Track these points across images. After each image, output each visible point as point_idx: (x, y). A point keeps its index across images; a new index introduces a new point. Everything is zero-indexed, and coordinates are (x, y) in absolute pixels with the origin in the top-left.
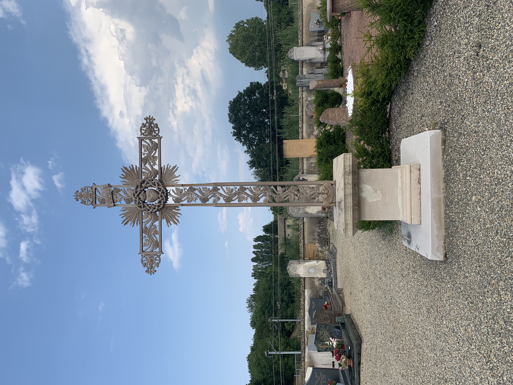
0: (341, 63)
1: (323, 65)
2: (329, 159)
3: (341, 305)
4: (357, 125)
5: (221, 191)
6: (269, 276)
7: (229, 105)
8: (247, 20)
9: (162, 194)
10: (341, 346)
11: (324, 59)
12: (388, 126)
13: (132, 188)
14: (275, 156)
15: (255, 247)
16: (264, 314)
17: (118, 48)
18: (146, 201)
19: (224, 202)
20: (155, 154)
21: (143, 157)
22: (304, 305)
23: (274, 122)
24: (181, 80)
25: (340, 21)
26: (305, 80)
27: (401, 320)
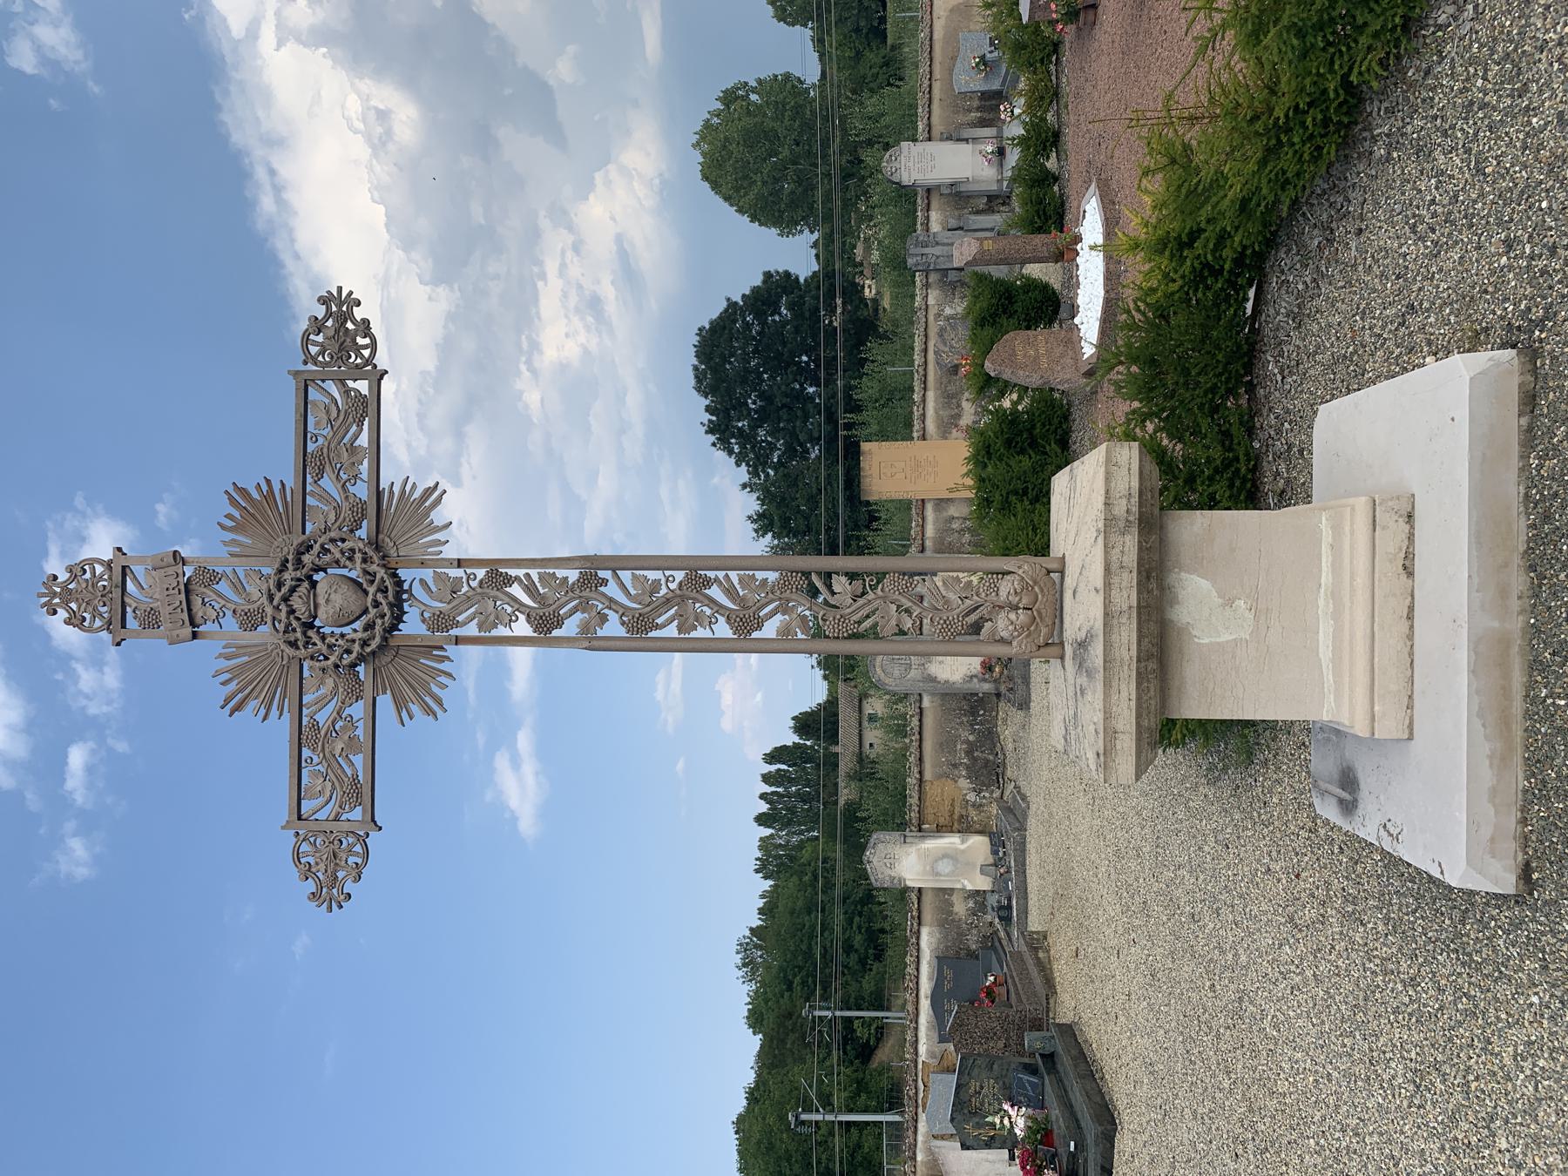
0: (1056, 188)
1: (995, 201)
2: (1013, 498)
3: (1041, 990)
4: (1134, 360)
5: (612, 590)
6: (809, 870)
7: (696, 340)
8: (760, 81)
9: (380, 597)
10: (1042, 1134)
11: (1000, 181)
12: (1249, 368)
13: (266, 571)
14: (834, 501)
15: (767, 778)
16: (790, 988)
17: (371, 169)
18: (317, 623)
19: (621, 632)
20: (356, 436)
21: (311, 447)
22: (917, 978)
23: (834, 396)
24: (557, 264)
25: (1056, 46)
26: (937, 250)
27: (1283, 1087)
